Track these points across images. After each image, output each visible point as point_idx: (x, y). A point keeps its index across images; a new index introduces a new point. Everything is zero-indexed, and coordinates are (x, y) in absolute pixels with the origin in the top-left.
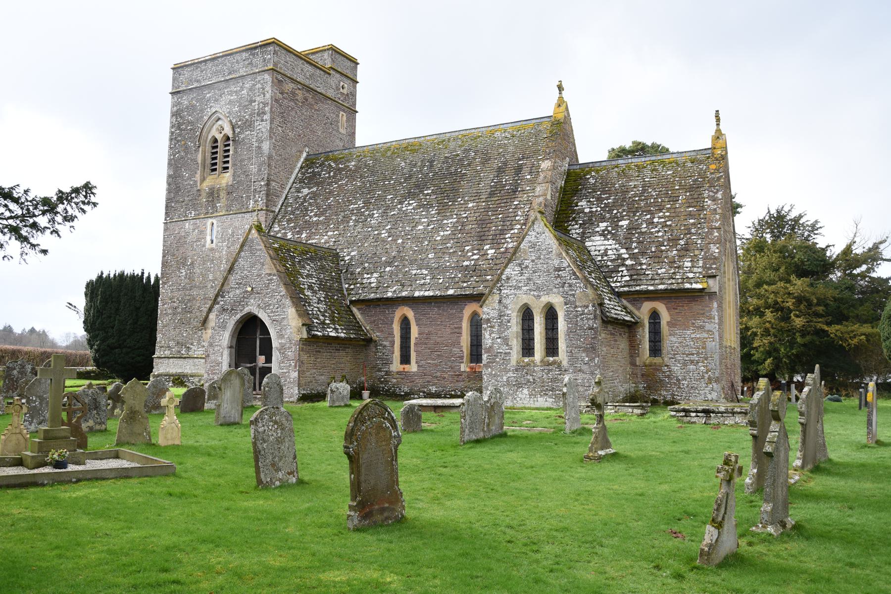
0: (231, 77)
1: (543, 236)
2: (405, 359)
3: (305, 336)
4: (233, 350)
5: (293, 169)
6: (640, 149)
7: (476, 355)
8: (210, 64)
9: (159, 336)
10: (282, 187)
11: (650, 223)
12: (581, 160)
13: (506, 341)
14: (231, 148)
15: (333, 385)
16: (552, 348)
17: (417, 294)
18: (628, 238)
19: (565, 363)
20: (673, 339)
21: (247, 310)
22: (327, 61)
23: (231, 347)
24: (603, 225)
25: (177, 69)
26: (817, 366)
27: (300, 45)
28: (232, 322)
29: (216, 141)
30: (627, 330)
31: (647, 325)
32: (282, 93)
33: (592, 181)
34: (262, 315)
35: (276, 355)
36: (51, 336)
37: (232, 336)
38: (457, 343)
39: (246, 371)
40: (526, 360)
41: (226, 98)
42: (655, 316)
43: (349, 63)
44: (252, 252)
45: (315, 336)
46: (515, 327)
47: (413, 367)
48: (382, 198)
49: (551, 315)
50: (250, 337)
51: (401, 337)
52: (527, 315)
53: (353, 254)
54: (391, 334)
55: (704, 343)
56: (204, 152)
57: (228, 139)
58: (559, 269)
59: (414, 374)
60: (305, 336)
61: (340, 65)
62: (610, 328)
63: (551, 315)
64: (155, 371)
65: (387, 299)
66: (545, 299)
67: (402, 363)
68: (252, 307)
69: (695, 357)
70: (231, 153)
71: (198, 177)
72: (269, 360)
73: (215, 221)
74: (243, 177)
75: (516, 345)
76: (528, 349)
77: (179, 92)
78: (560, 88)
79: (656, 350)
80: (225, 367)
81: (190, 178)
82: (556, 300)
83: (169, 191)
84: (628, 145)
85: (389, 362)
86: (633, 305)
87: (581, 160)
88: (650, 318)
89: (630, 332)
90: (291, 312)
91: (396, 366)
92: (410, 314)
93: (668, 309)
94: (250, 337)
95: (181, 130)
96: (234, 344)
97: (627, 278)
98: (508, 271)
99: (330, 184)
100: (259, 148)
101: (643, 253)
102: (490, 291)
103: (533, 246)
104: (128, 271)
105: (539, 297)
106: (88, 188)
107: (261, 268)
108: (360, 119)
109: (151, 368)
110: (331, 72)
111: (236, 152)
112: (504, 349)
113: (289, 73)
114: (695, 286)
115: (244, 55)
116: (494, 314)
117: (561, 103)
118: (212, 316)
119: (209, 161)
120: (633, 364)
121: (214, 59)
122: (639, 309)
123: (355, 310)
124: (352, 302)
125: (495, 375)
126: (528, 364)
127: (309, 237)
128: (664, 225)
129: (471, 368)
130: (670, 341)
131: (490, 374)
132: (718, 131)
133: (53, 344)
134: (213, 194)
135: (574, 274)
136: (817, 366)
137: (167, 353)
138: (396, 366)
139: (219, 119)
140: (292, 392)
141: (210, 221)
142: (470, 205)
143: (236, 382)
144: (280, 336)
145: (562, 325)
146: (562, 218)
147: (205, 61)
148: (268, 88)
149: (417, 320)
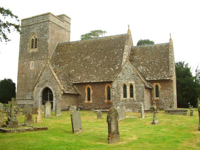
0: (38, 22)
2: (89, 99)
4: (42, 97)
7: (109, 98)
8: (32, 19)
10: (52, 52)
11: (154, 62)
13: (119, 94)
14: (38, 42)
16: (132, 95)
17: (92, 81)
19: (135, 99)
21: (46, 86)
23: (41, 96)
28: (41, 89)
29: (33, 40)
30: (149, 90)
31: (155, 89)
34: (50, 88)
40: (125, 99)
41: (36, 28)
42: (157, 86)
43: (68, 19)
47: (91, 101)
48: (80, 56)
49: (131, 87)
51: (88, 93)
53: (73, 70)
54: (85, 93)
55: (170, 93)
56: (30, 43)
57: (36, 39)
63: (131, 87)
65: (91, 82)
66: (130, 82)
68: (47, 85)
69: (168, 97)
73: (33, 62)
74: (41, 50)
75: (122, 95)
76: (125, 96)
77: (23, 27)
85: (84, 100)
86: (151, 84)
88: (156, 87)
89: (150, 91)
91: (86, 101)
92: (90, 87)
95: (23, 37)
96: (42, 96)
99: (65, 52)
102: (114, 80)
104: (143, 39)
110: (64, 21)
111: (39, 42)
112: (119, 96)
113: (53, 22)
114: (167, 79)
115: (41, 17)
118: (35, 88)
119: (31, 45)
120: (151, 99)
121: (33, 18)
122: (153, 85)
125: (116, 103)
130: (161, 93)
131: (115, 103)
139: (34, 34)
141: (31, 62)
142: (105, 57)
144: (55, 93)
145: (134, 89)
147: (30, 18)
149: (92, 89)
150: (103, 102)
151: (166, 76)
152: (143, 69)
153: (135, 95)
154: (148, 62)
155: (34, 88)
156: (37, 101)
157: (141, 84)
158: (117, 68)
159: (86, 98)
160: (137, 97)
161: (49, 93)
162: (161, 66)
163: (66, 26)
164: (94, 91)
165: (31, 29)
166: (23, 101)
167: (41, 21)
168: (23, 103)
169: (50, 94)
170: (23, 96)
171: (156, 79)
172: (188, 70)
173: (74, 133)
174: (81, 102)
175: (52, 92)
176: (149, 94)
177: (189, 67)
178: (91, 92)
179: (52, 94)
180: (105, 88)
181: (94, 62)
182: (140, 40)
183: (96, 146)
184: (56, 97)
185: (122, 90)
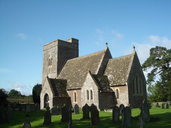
8: (49, 45)
13: (85, 97)
16: (92, 98)
20: (121, 95)
21: (46, 92)
26: (90, 112)
32: (60, 49)
34: (48, 93)
46: (86, 94)
52: (88, 92)
68: (46, 92)
71: (47, 66)
75: (86, 98)
76: (88, 99)
78: (107, 44)
81: (46, 67)
105: (89, 88)
116: (83, 92)
127: (63, 77)
128: (121, 71)
136: (90, 112)
144: (50, 97)
148: (57, 49)
152: (111, 77)
159: (74, 100)
160: (94, 99)
163: (74, 46)
164: (78, 95)
167: (54, 46)
171: (115, 85)
182: (36, 84)
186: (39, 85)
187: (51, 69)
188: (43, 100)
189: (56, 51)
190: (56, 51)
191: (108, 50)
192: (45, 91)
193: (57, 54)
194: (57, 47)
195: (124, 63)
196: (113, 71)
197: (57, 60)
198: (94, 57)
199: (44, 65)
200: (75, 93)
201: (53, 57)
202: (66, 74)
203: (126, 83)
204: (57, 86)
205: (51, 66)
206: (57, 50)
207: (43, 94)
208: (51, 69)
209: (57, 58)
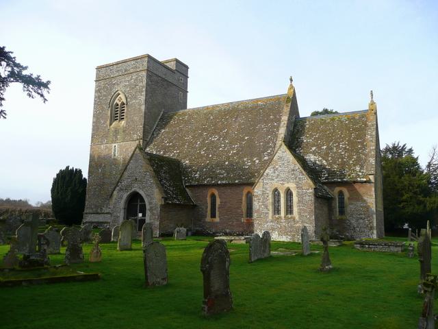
1: (284, 153)
3: (163, 203)
5: (156, 118)
6: (326, 112)
8: (115, 67)
9: (87, 203)
11: (338, 147)
12: (301, 116)
13: (266, 207)
15: (177, 229)
17: (219, 182)
18: (327, 154)
19: (297, 218)
21: (133, 189)
22: (172, 66)
24: (314, 148)
25: (99, 69)
27: (160, 59)
28: (125, 196)
31: (337, 199)
33: (307, 126)
34: (141, 192)
35: (148, 213)
36: (30, 203)
37: (126, 203)
38: (240, 208)
39: (133, 221)
42: (341, 193)
43: (184, 68)
44: (137, 161)
45: (168, 203)
47: (217, 219)
50: (135, 203)
52: (276, 193)
58: (293, 170)
59: (217, 223)
60: (163, 203)
61: (181, 70)
62: (320, 200)
63: (289, 193)
64: (84, 221)
66: (287, 185)
67: (211, 217)
68: (136, 188)
69: (363, 216)
70: (125, 111)
71: (108, 122)
72: (144, 215)
76: (277, 210)
78: (291, 80)
79: (342, 212)
80: (121, 220)
82: (292, 186)
83: (93, 130)
84: (320, 110)
87: (301, 116)
88: (339, 195)
90: (284, 239)
92: (216, 193)
93: (348, 191)
94: (135, 203)
97: (327, 175)
98: (267, 171)
100: (140, 108)
101: (335, 163)
103: (280, 158)
105: (283, 184)
106: (46, 85)
107: (142, 169)
108: (189, 95)
109: (82, 218)
113: (155, 72)
114: (362, 179)
115: (133, 62)
117: (292, 87)
118: (115, 193)
120: (330, 219)
121: (117, 64)
122: (333, 191)
123: (187, 190)
124: (187, 186)
126: (278, 219)
127: (164, 153)
128: (345, 148)
129: (247, 220)
132: (372, 101)
133: (30, 206)
134: (116, 131)
135: (302, 172)
137: (91, 211)
138: (208, 219)
140: (157, 233)
141: (114, 145)
143: (129, 227)
144: (150, 203)
145: (295, 199)
146: (293, 142)
148: (145, 79)
150: (237, 220)
151: (360, 174)
153: (295, 209)
154: (325, 147)
155: (113, 192)
156: (118, 217)
157: (308, 189)
158: (265, 158)
160: (300, 213)
161: (139, 203)
162: (350, 157)
165: (114, 84)
166: (97, 216)
167: (132, 71)
168: (96, 220)
169: (140, 205)
170: (96, 207)
172: (414, 162)
173: (49, 82)
174: (200, 221)
175: (144, 202)
176: (326, 209)
177: (415, 156)
178: (218, 201)
179: (145, 205)
180: (242, 195)
181: (225, 147)
183: (181, 245)
184: (151, 209)
185: (270, 200)
186: (72, 170)
187: (121, 131)
188: (122, 211)
189: (141, 84)
190: (141, 84)
191: (373, 103)
192: (130, 186)
193: (144, 93)
194: (144, 74)
195: (349, 131)
196: (319, 147)
197: (143, 108)
198: (252, 108)
199: (98, 119)
200: (213, 196)
201: (128, 100)
202: (174, 146)
203: (372, 178)
204: (164, 173)
205: (123, 122)
206: (145, 83)
207: (121, 193)
208: (121, 131)
209: (143, 102)
